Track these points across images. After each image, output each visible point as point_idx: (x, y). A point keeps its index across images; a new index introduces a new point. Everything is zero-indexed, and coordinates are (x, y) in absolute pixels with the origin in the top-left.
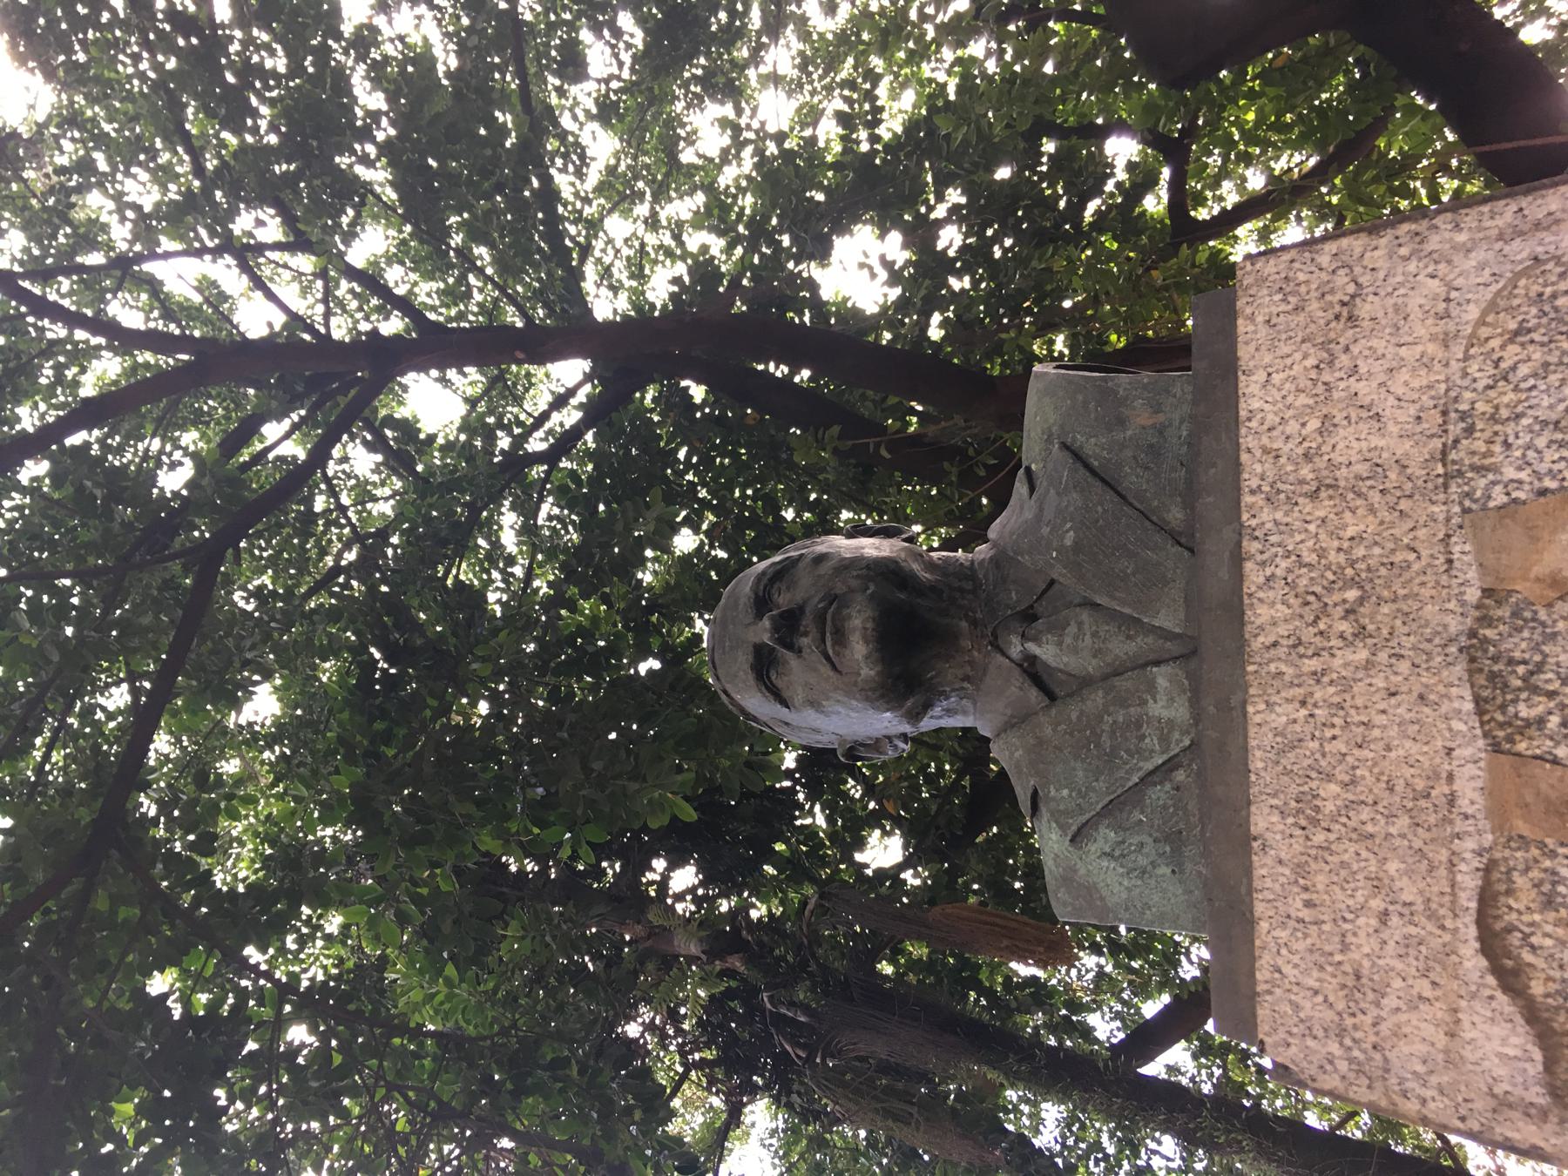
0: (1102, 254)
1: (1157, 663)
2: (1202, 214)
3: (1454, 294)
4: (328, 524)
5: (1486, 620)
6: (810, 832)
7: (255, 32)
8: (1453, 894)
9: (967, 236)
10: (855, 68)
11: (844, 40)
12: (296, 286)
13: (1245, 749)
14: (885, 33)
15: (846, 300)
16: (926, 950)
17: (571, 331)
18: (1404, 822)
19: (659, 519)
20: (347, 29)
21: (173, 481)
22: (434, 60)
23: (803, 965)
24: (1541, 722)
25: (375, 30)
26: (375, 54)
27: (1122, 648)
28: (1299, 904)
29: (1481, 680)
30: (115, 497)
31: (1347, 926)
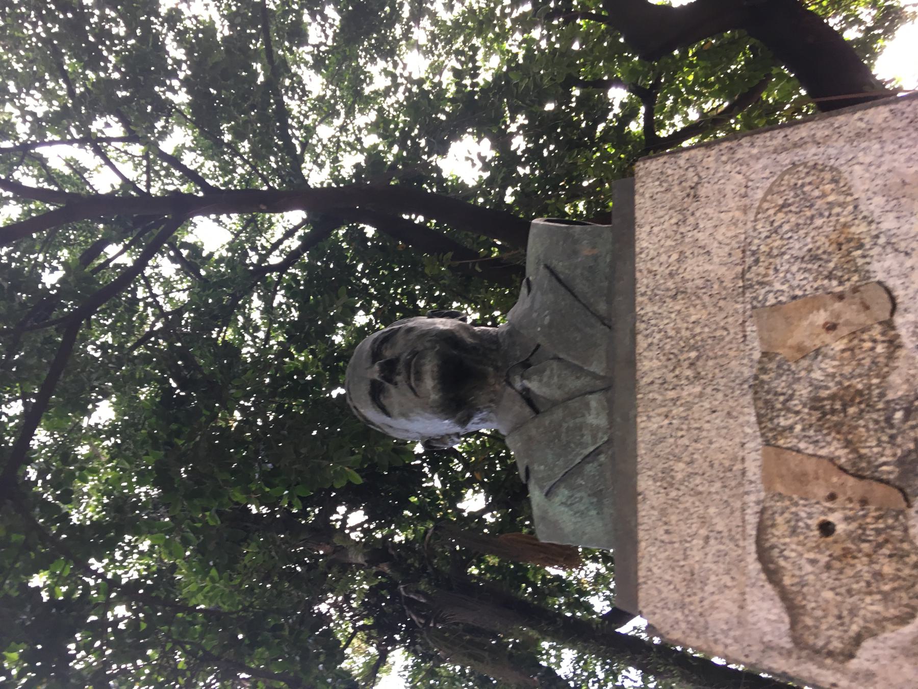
0: (606, 156)
1: (591, 393)
2: (663, 134)
3: (750, 184)
4: (147, 305)
5: (763, 370)
6: (431, 491)
7: (107, 11)
8: (744, 527)
9: (528, 142)
10: (464, 42)
11: (458, 27)
12: (130, 164)
13: (635, 442)
14: (481, 23)
15: (458, 179)
16: (497, 560)
17: (295, 193)
18: (718, 485)
19: (345, 306)
20: (163, 11)
21: (50, 279)
22: (214, 31)
23: (424, 569)
24: (791, 428)
25: (179, 12)
26: (180, 26)
27: (575, 384)
28: (662, 532)
29: (760, 404)
30: (16, 287)
31: (687, 545)
